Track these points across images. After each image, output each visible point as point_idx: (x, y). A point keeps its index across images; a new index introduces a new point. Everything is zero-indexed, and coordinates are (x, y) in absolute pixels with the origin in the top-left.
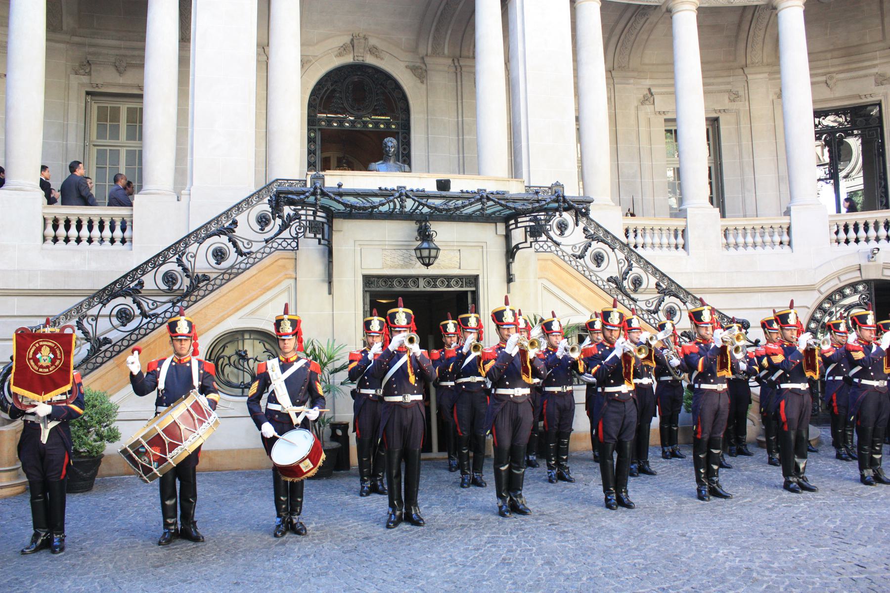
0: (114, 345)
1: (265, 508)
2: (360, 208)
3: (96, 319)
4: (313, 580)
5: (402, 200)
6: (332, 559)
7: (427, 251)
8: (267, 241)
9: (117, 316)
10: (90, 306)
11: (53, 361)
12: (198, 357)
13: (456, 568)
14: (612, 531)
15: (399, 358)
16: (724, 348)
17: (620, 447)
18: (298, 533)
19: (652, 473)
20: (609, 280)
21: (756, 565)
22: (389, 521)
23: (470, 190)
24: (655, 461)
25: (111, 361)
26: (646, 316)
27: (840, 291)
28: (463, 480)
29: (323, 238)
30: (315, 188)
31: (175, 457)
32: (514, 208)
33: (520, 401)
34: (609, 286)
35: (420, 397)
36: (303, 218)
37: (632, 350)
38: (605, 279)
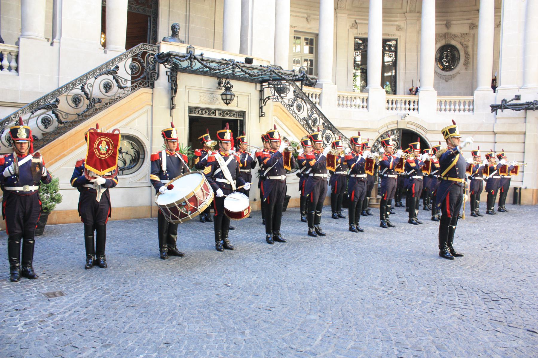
11: (107, 151)
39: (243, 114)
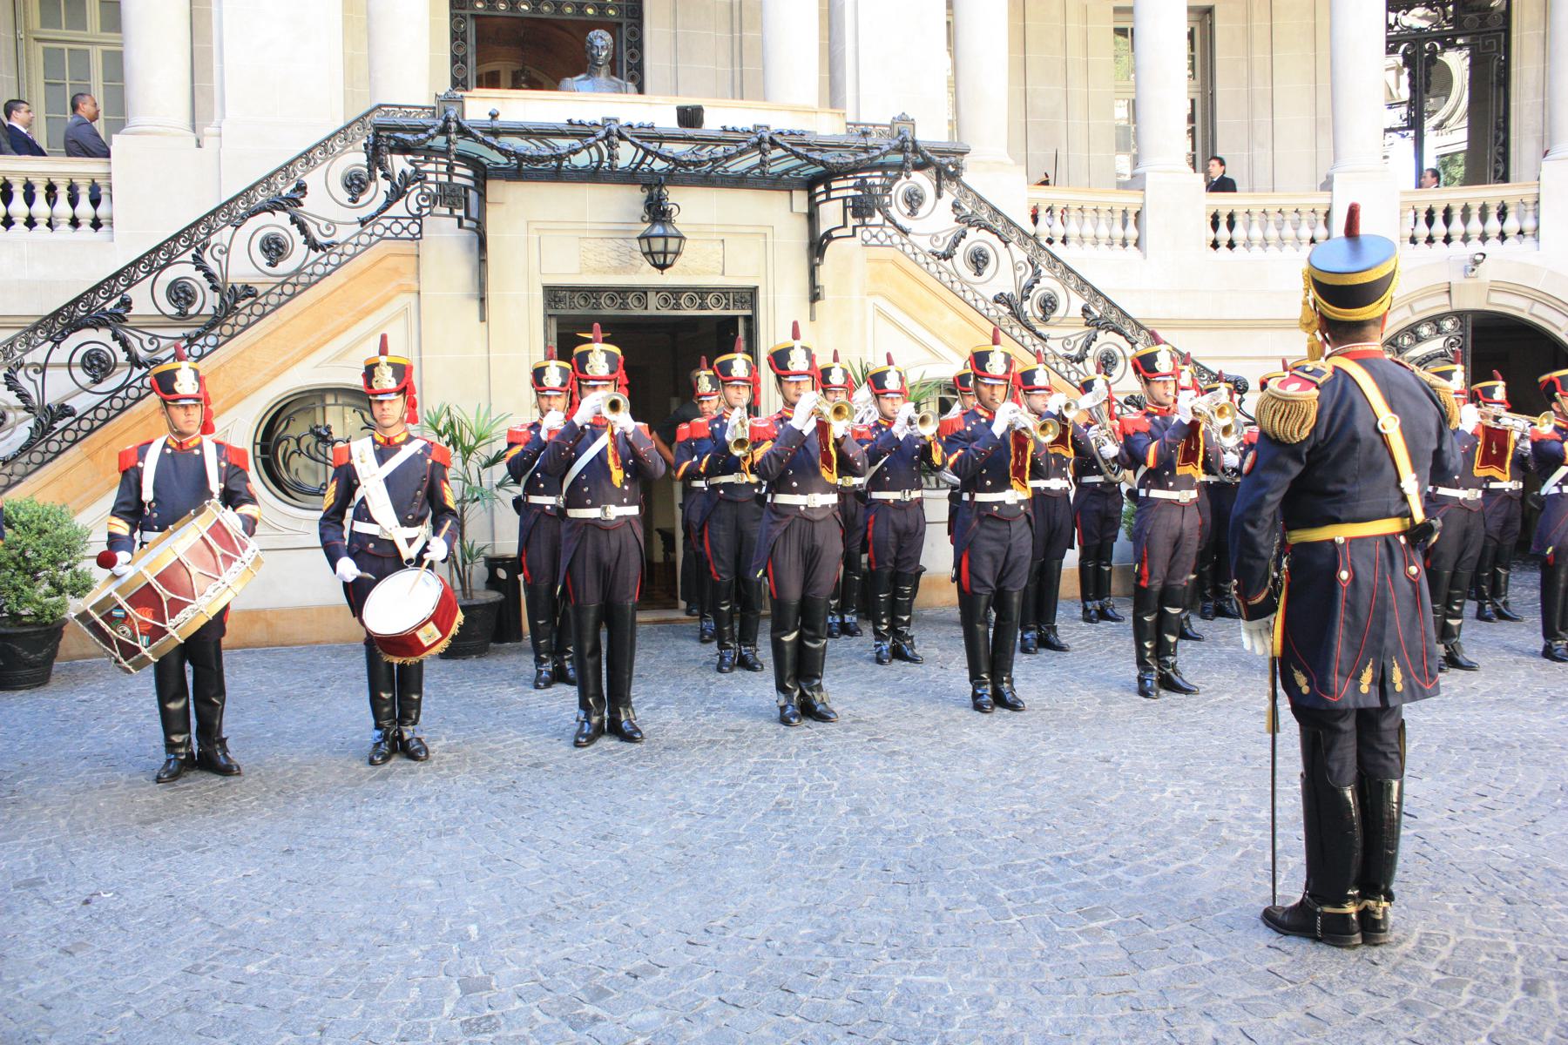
0: (81, 418)
1: (353, 712)
2: (531, 159)
3: (43, 370)
4: (427, 844)
5: (610, 146)
6: (468, 804)
7: (662, 241)
8: (363, 223)
9: (83, 365)
10: (30, 346)
12: (214, 436)
13: (690, 821)
14: (979, 751)
15: (595, 438)
16: (1194, 426)
17: (1000, 600)
18: (413, 756)
19: (1060, 648)
20: (996, 300)
21: (1226, 816)
22: (579, 734)
23: (739, 128)
24: (1068, 622)
25: (76, 447)
26: (1062, 367)
27: (1412, 330)
28: (722, 658)
29: (467, 217)
30: (447, 120)
31: (180, 627)
32: (822, 163)
33: (817, 517)
34: (998, 310)
35: (634, 510)
36: (431, 177)
37: (1031, 427)
38: (991, 299)
39: (749, 296)
